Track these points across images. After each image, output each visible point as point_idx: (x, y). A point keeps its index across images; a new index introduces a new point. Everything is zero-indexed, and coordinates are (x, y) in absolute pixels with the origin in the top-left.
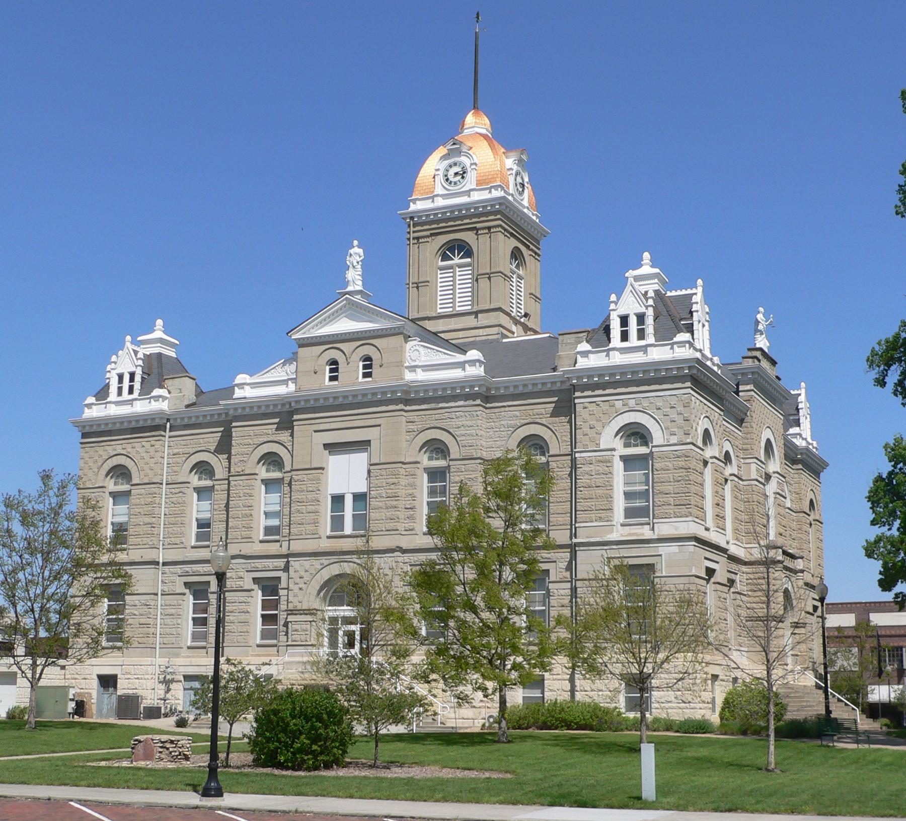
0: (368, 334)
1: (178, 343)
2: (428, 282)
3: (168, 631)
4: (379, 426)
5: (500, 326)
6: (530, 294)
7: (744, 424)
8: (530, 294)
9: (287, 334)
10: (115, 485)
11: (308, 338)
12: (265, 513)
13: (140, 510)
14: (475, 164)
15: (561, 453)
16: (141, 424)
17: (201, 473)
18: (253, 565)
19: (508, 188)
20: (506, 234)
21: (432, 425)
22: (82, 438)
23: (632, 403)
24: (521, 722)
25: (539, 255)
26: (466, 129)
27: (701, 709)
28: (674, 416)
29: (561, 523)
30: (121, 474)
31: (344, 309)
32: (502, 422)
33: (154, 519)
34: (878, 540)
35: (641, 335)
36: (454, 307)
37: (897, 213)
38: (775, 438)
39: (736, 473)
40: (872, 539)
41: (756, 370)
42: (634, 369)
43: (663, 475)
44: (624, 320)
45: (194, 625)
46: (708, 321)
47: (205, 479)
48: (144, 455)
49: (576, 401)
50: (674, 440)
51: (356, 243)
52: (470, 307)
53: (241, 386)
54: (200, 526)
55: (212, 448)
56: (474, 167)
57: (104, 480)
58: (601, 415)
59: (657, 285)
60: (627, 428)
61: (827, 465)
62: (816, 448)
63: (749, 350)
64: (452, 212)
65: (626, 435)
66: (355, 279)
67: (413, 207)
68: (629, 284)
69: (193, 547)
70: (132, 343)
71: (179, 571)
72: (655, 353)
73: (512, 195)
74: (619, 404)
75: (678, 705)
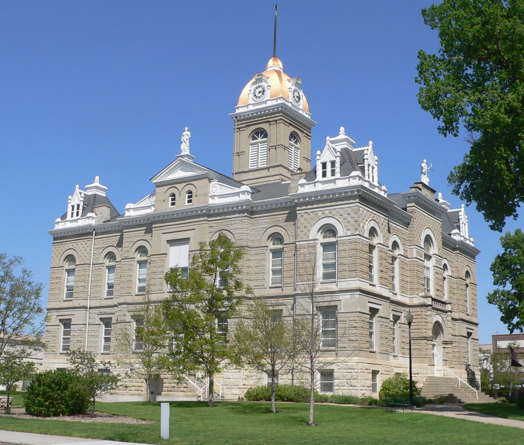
0: (190, 179)
1: (107, 189)
2: (244, 152)
3: (91, 344)
4: (194, 229)
5: (281, 175)
6: (304, 157)
7: (409, 226)
8: (304, 157)
9: (150, 180)
10: (69, 265)
11: (160, 182)
12: (139, 280)
13: (79, 279)
14: (270, 86)
15: (290, 242)
16: (81, 232)
17: (110, 258)
18: (131, 308)
19: (288, 99)
20: (286, 124)
21: (222, 229)
22: (54, 240)
23: (327, 212)
24: (258, 396)
25: (310, 136)
26: (269, 68)
27: (361, 390)
28: (349, 219)
29: (289, 283)
30: (72, 259)
31: (179, 165)
32: (260, 226)
33: (85, 284)
34: (496, 293)
35: (333, 173)
36: (258, 167)
37: (416, 81)
38: (434, 235)
39: (403, 254)
40: (492, 292)
41: (416, 194)
42: (327, 192)
43: (343, 254)
44: (324, 165)
45: (105, 341)
46: (377, 165)
47: (112, 262)
48: (82, 249)
49: (297, 212)
50: (349, 233)
51: (186, 129)
52: (266, 165)
53: (128, 210)
54: (109, 287)
55: (115, 245)
56: (269, 87)
57: (63, 263)
58: (310, 220)
59: (346, 145)
60: (324, 227)
61: (480, 252)
62: (473, 242)
63: (415, 183)
64: (257, 113)
65: (324, 231)
66: (185, 149)
67: (237, 111)
68: (327, 144)
69: (105, 299)
70: (79, 189)
71: (98, 312)
72: (340, 183)
73: (291, 103)
74: (320, 213)
75: (349, 388)
